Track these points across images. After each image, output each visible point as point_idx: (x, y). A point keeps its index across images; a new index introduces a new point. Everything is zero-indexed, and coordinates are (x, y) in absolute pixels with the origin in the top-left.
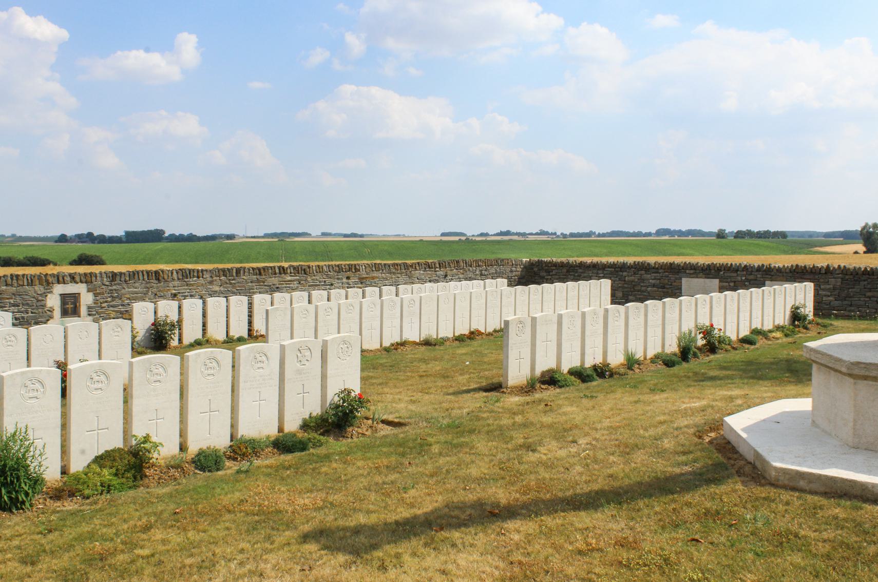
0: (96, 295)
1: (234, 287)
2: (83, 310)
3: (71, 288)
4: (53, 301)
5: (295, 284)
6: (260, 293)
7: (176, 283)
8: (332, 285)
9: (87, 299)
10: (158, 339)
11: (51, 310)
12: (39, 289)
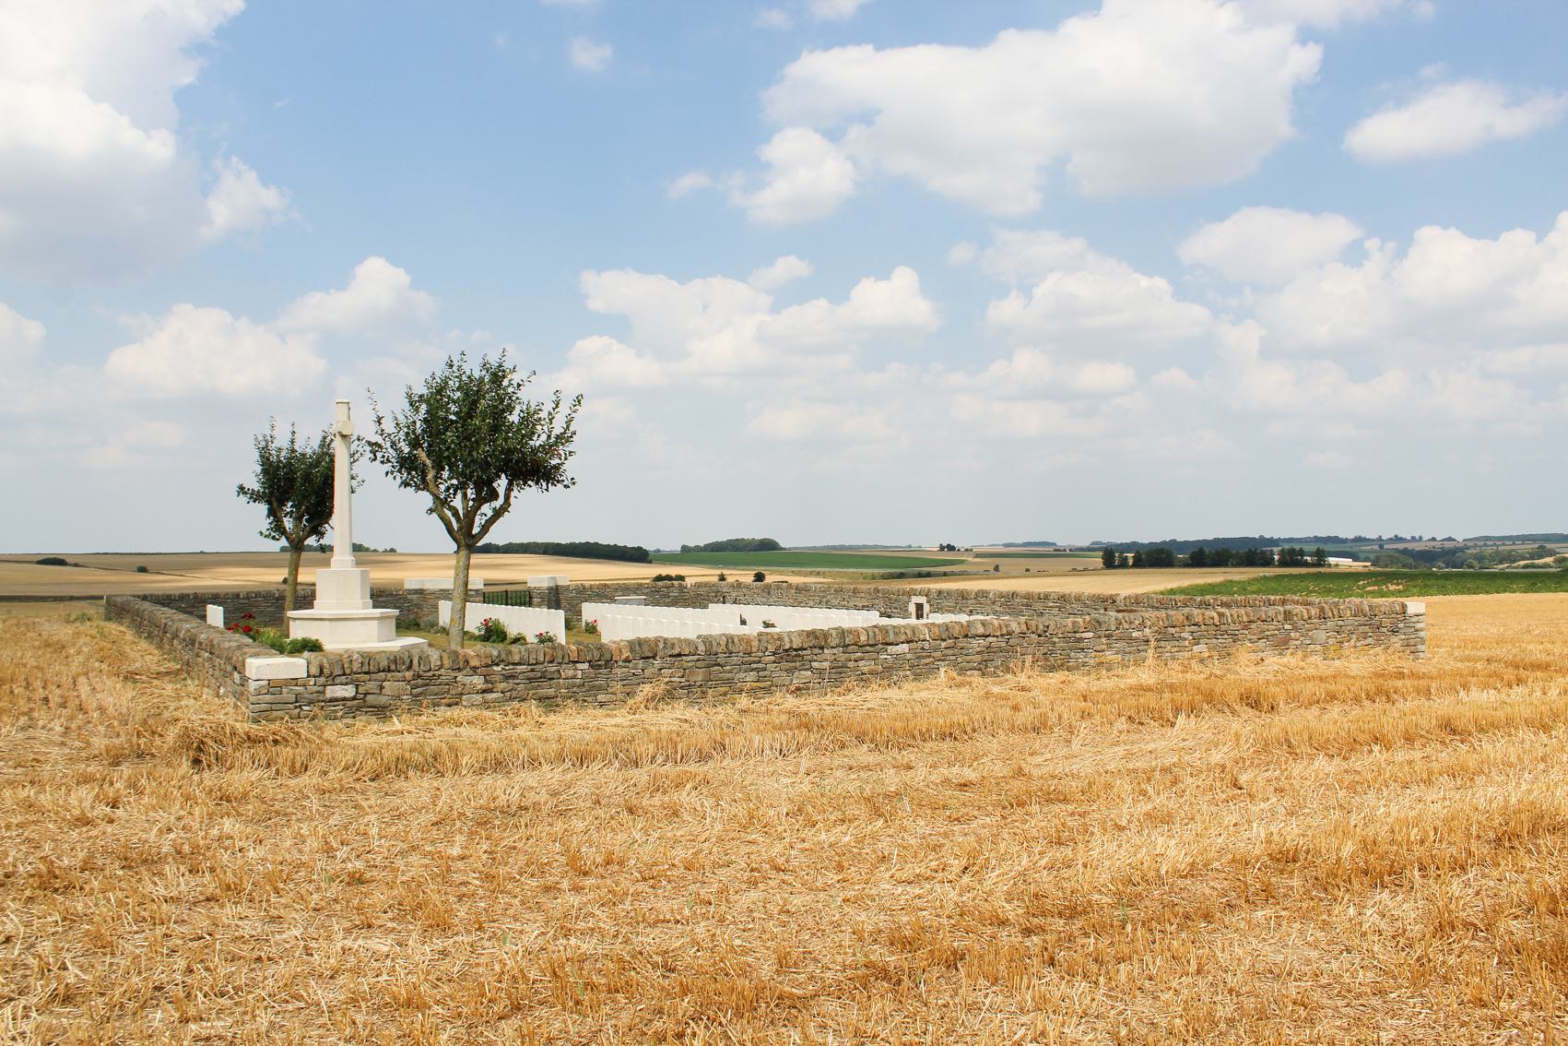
4: (912, 608)
9: (926, 608)
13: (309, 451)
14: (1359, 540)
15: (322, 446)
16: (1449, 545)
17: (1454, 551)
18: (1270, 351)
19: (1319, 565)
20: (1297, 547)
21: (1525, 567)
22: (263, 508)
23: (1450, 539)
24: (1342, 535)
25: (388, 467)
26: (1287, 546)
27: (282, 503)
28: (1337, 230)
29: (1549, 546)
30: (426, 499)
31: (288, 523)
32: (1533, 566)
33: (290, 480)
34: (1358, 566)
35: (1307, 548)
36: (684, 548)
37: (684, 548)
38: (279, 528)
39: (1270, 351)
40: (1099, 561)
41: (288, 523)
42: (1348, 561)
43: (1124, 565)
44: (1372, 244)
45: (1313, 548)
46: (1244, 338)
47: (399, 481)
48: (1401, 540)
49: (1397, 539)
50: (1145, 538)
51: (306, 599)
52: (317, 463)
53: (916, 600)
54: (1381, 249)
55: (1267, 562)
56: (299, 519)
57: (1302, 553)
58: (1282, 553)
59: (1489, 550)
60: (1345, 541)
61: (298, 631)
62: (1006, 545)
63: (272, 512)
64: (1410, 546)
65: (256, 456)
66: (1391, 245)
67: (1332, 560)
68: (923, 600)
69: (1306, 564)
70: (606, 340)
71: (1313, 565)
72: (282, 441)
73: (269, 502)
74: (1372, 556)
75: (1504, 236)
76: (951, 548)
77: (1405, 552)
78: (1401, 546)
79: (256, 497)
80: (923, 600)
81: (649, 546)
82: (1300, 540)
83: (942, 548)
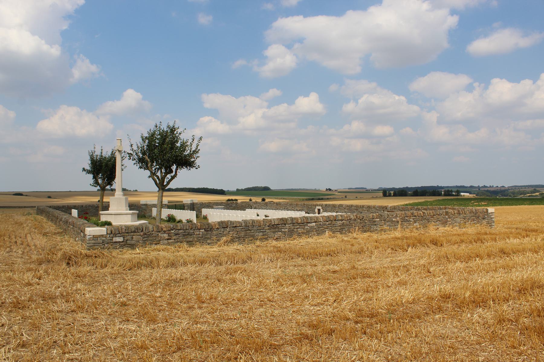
4: (316, 211)
9: (321, 210)
13: (107, 156)
14: (471, 187)
15: (112, 154)
16: (503, 189)
17: (504, 191)
18: (441, 122)
19: (458, 196)
20: (450, 189)
21: (529, 196)
22: (91, 176)
23: (503, 187)
24: (466, 185)
25: (135, 162)
26: (446, 189)
27: (98, 174)
28: (464, 80)
29: (537, 189)
30: (148, 173)
31: (100, 181)
32: (532, 196)
33: (101, 166)
34: (471, 196)
35: (453, 190)
36: (237, 190)
37: (237, 190)
38: (97, 183)
39: (441, 122)
41: (100, 181)
42: (468, 194)
43: (390, 195)
44: (476, 84)
45: (456, 190)
46: (432, 117)
47: (138, 166)
48: (486, 187)
49: (485, 187)
50: (397, 186)
51: (106, 207)
52: (110, 160)
53: (318, 207)
54: (479, 86)
55: (439, 194)
56: (104, 180)
57: (452, 191)
58: (445, 191)
59: (517, 190)
60: (467, 187)
61: (103, 219)
62: (349, 189)
63: (94, 177)
64: (489, 189)
65: (89, 158)
66: (483, 85)
67: (462, 194)
68: (320, 208)
69: (453, 195)
70: (210, 118)
71: (456, 196)
72: (98, 153)
73: (93, 174)
74: (476, 193)
75: (522, 82)
76: (330, 190)
77: (487, 191)
78: (486, 189)
79: (89, 172)
80: (320, 208)
81: (225, 189)
82: (451, 187)
83: (327, 190)
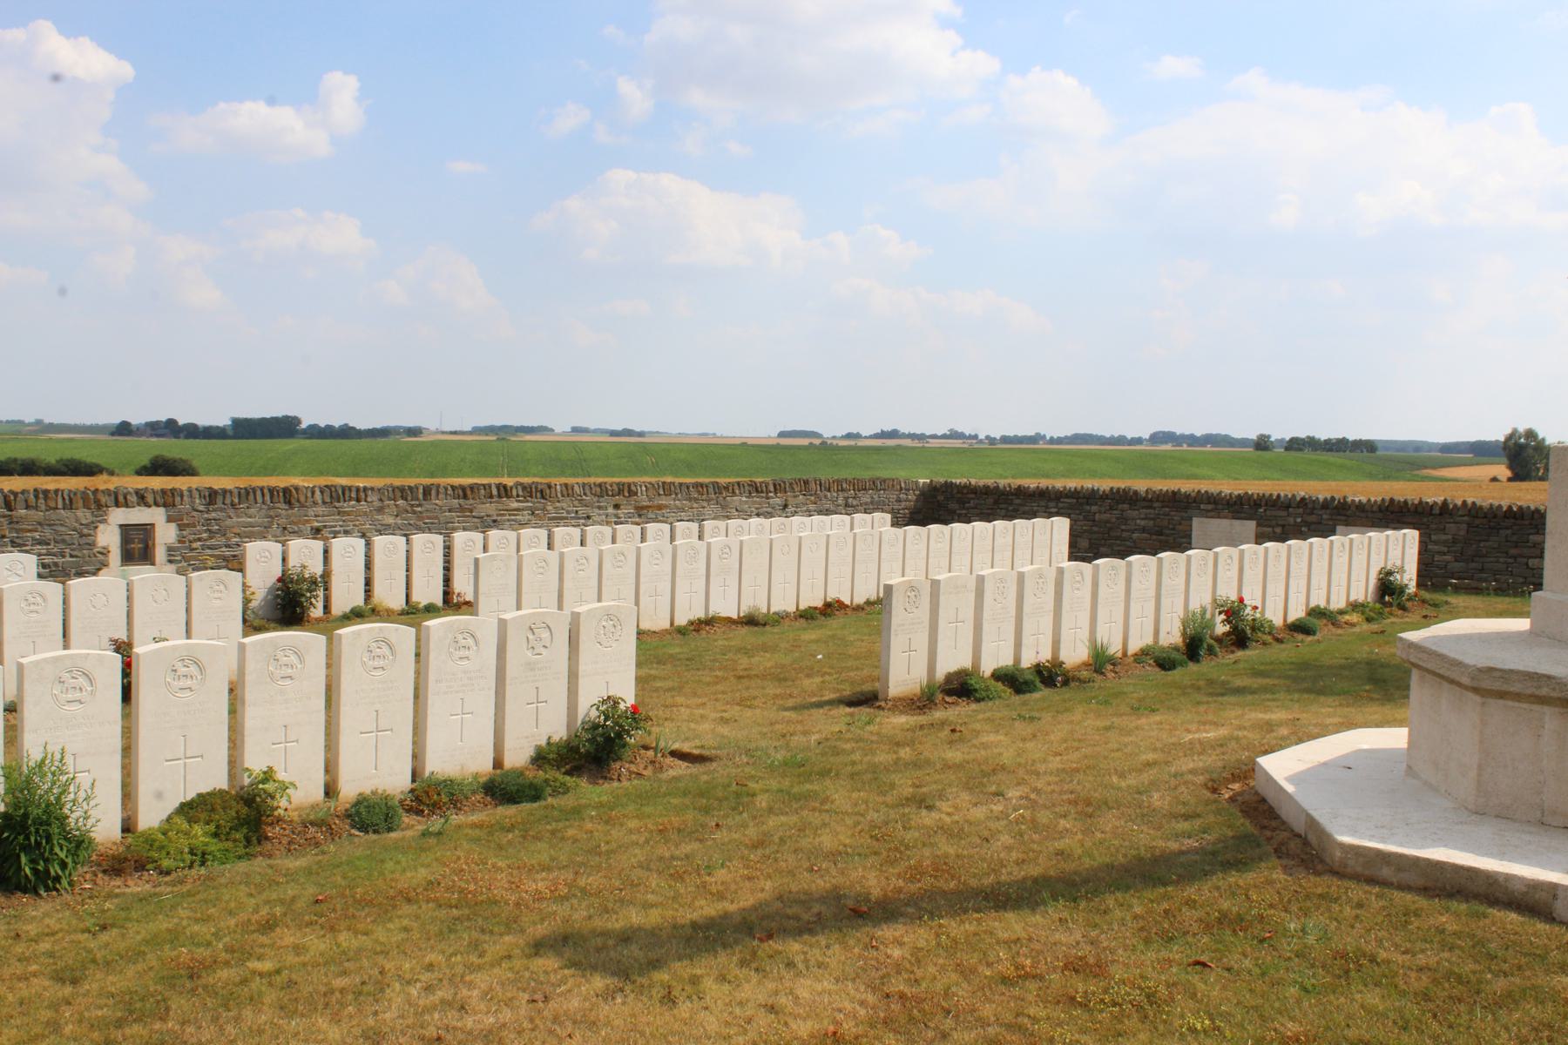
0: (181, 528)
1: (420, 518)
2: (160, 554)
3: (138, 515)
4: (108, 537)
5: (525, 516)
6: (465, 529)
7: (320, 510)
8: (589, 517)
9: (165, 534)
10: (289, 606)
11: (105, 552)
12: (84, 515)
40: (1503, 471)
53: (119, 516)
68: (154, 516)
